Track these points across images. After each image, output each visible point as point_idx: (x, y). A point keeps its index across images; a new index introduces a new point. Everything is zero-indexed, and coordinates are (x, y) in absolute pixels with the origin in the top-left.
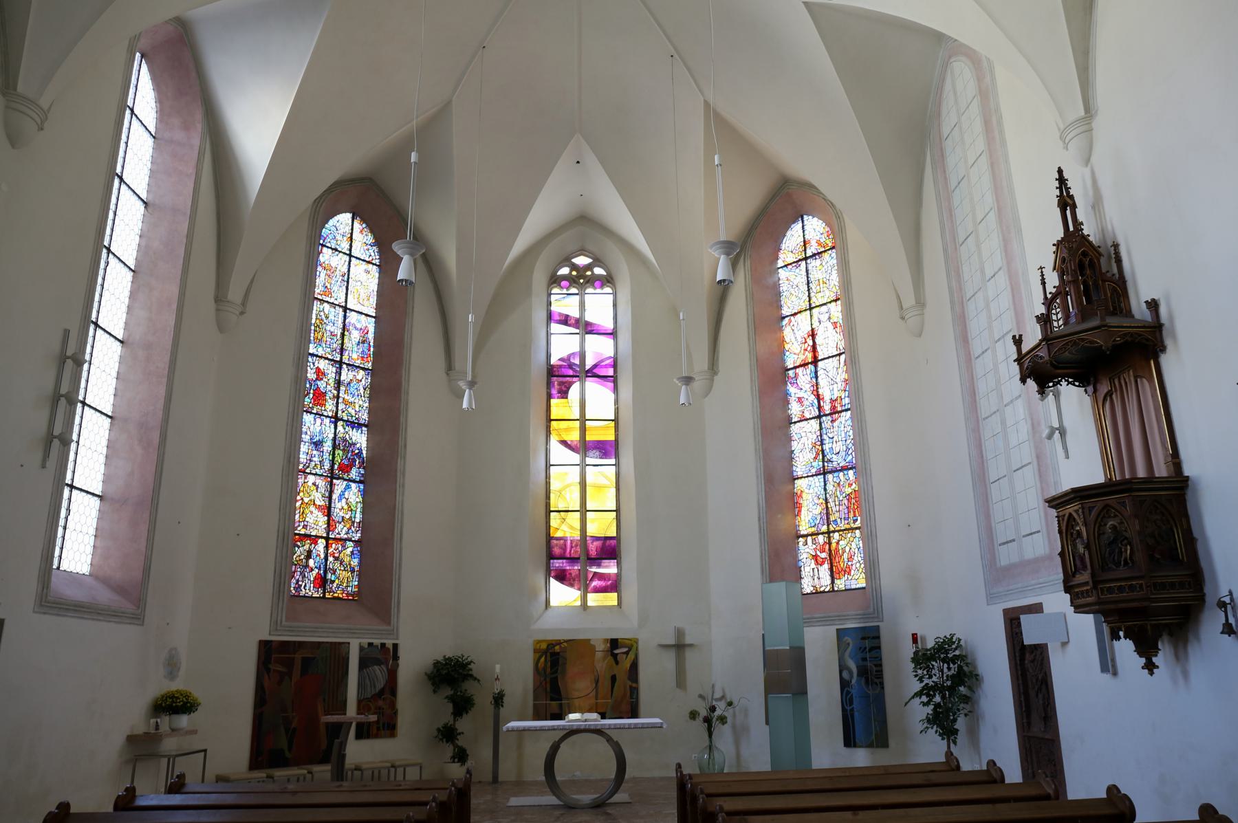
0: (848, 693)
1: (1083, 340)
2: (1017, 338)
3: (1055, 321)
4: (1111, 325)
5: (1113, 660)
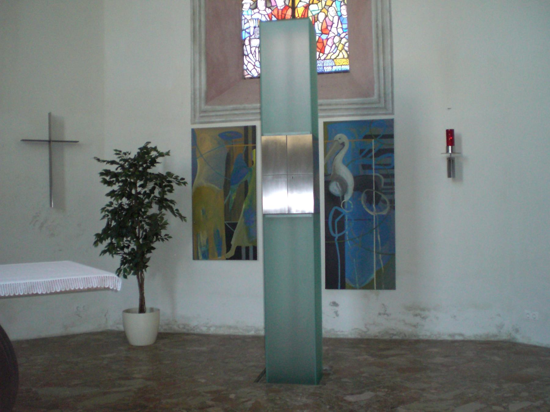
0: (337, 213)
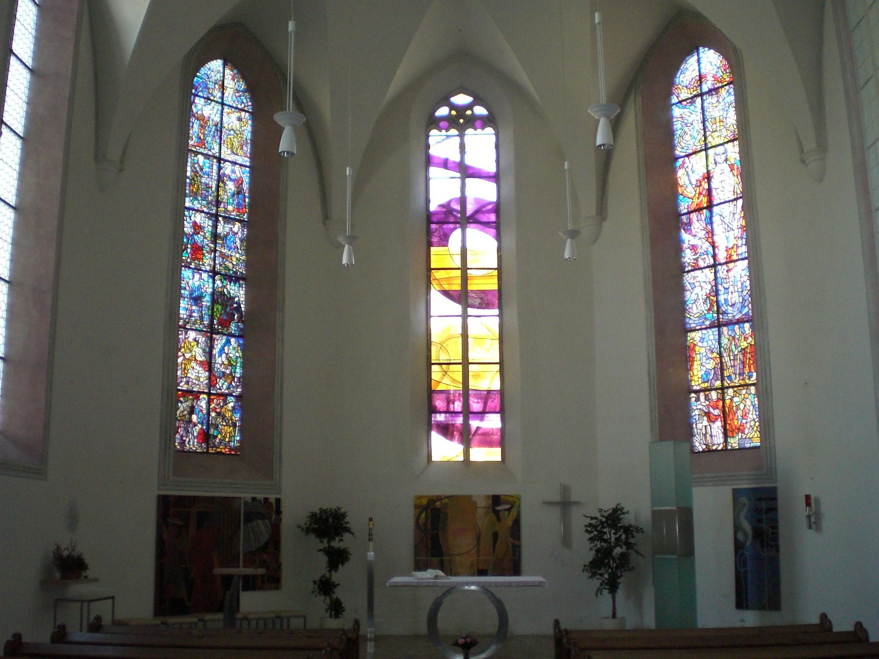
0: (742, 554)
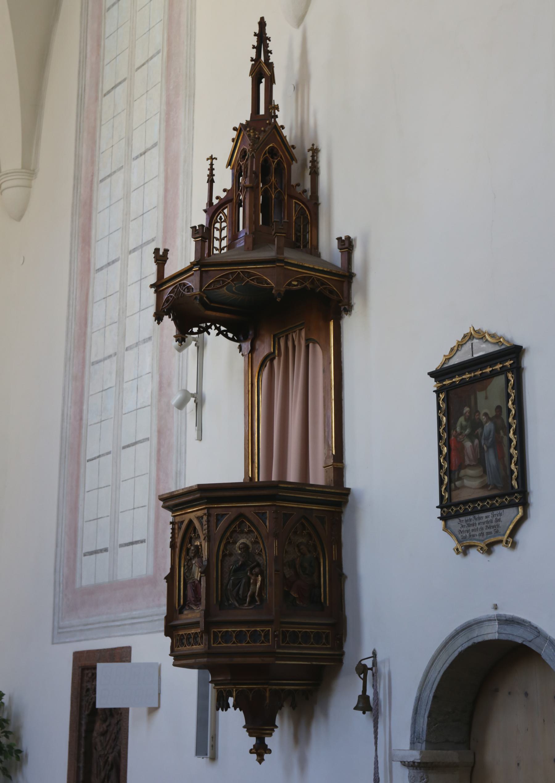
1: (249, 275)
2: (161, 253)
3: (217, 239)
4: (289, 261)
5: (214, 738)
